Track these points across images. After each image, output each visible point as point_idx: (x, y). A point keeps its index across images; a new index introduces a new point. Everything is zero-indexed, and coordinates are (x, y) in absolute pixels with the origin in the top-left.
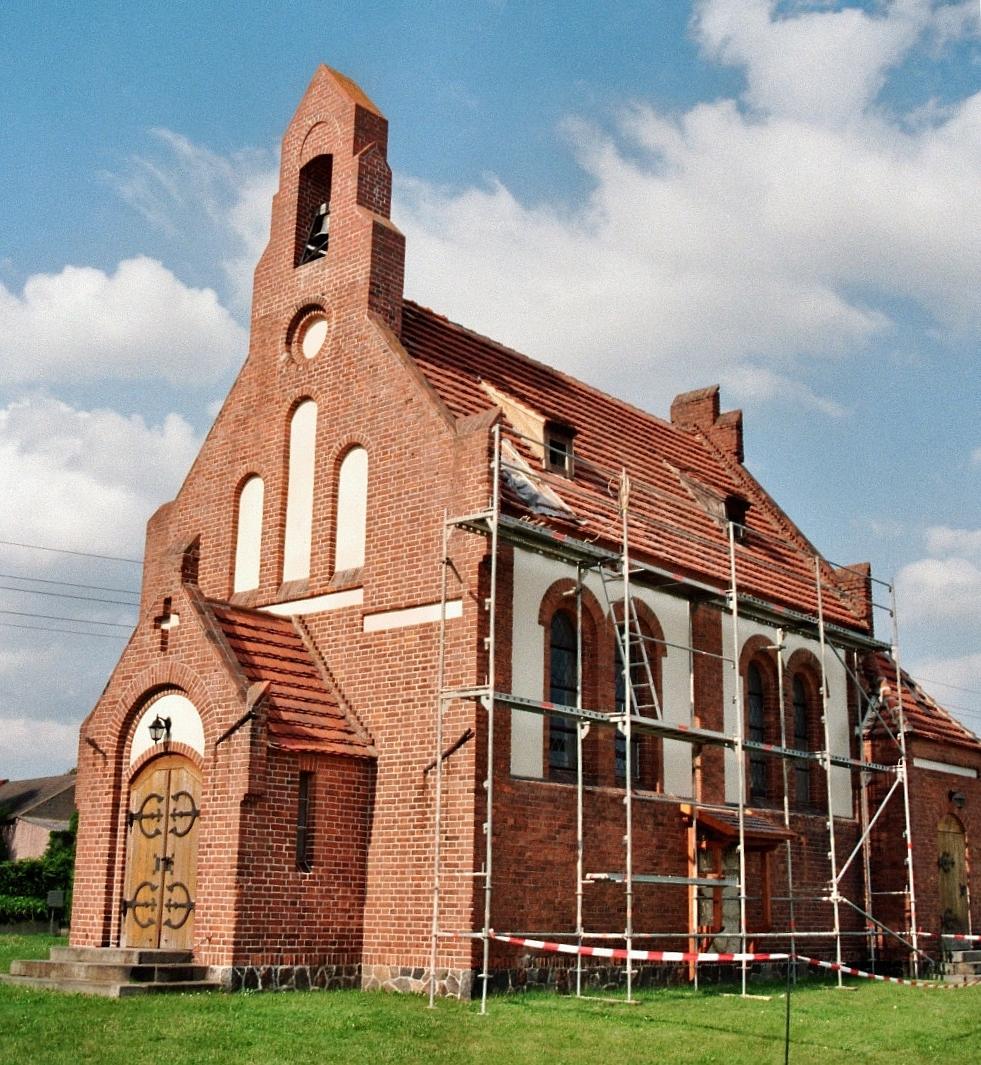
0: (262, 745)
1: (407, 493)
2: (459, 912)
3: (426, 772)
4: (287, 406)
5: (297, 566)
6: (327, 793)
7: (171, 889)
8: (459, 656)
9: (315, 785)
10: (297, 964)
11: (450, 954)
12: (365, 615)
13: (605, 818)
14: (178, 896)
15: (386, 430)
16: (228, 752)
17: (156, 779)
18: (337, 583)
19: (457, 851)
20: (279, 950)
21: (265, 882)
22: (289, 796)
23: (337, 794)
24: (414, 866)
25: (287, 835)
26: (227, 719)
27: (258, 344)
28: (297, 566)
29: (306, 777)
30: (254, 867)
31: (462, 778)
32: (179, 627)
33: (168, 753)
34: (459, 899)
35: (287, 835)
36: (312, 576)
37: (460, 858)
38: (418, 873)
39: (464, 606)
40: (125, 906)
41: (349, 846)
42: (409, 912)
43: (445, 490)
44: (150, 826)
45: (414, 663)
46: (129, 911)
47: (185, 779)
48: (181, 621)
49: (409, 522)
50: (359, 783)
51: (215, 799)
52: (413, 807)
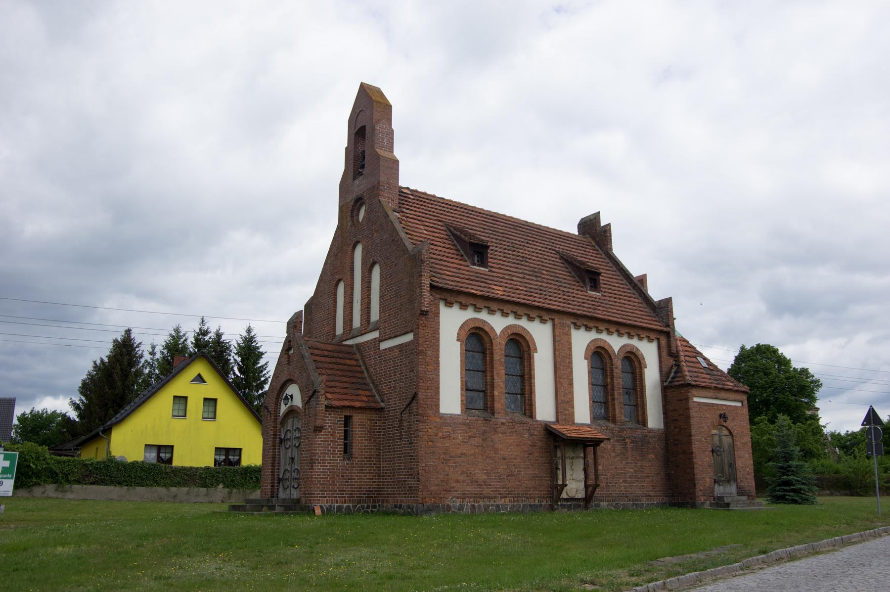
5: (357, 323)
12: (381, 341)
14: (295, 475)
18: (371, 327)
28: (357, 323)
29: (347, 420)
40: (280, 480)
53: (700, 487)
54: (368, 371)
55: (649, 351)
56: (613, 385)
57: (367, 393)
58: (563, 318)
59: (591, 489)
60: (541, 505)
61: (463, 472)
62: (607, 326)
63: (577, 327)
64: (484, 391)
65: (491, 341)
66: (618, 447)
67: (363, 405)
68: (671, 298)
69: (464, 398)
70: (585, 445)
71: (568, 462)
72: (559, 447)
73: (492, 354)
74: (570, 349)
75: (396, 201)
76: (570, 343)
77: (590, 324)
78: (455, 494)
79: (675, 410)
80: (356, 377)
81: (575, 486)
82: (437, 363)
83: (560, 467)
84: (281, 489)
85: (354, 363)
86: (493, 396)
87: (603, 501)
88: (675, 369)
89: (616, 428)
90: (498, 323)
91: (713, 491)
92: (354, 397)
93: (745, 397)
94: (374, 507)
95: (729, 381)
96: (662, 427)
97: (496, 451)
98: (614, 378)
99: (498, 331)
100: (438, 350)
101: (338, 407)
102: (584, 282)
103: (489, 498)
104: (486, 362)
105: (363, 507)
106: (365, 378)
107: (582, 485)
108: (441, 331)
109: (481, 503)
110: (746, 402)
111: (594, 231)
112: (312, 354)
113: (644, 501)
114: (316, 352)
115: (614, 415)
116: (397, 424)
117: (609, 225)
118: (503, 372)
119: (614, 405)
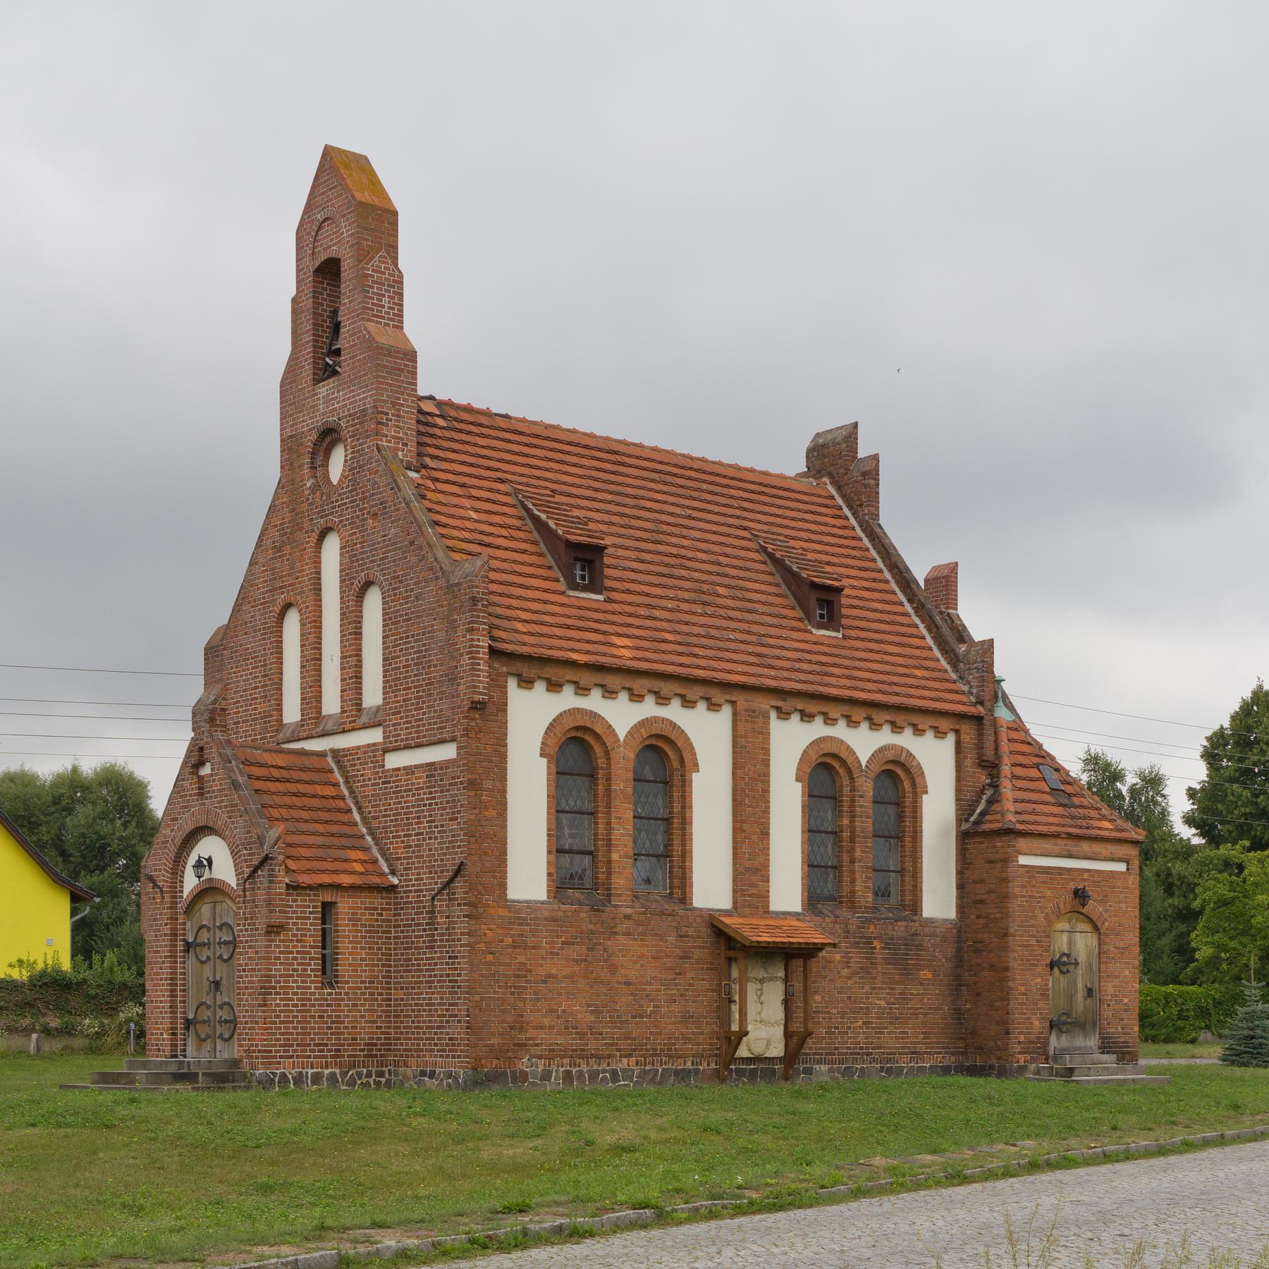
0: (280, 882)
1: (413, 636)
2: (459, 1022)
3: (433, 899)
4: (315, 536)
5: (331, 703)
6: (349, 920)
7: (221, 1007)
8: (456, 795)
9: (337, 913)
10: (327, 1067)
11: (453, 1057)
12: (386, 751)
13: (616, 933)
14: (223, 1014)
15: (395, 572)
16: (253, 889)
17: (205, 910)
19: (456, 969)
20: (309, 1057)
21: (292, 999)
22: (311, 924)
23: (360, 920)
24: (427, 982)
25: (311, 959)
26: (251, 860)
27: (288, 464)
28: (331, 703)
29: (327, 909)
30: (281, 988)
31: (459, 905)
32: (211, 775)
33: (210, 890)
34: (459, 1010)
35: (311, 959)
36: (343, 712)
37: (459, 975)
38: (430, 988)
39: (458, 748)
40: (188, 1023)
41: (374, 965)
42: (424, 1022)
43: (441, 635)
44: (205, 953)
45: (423, 799)
46: (191, 1027)
47: (227, 910)
48: (212, 770)
49: (416, 664)
50: (382, 909)
51: (246, 930)
52: (425, 930)
53: (1019, 1035)
54: (359, 809)
55: (935, 758)
56: (853, 832)
57: (360, 855)
58: (754, 698)
59: (796, 1040)
60: (697, 1071)
61: (551, 1011)
62: (846, 709)
63: (784, 715)
64: (590, 853)
65: (607, 753)
66: (857, 959)
67: (357, 880)
68: (991, 641)
69: (553, 871)
70: (793, 956)
71: (751, 988)
72: (736, 959)
73: (609, 779)
74: (766, 763)
75: (412, 447)
76: (766, 751)
77: (811, 708)
78: (534, 1050)
79: (982, 881)
80: (337, 823)
81: (764, 1031)
82: (502, 805)
83: (737, 998)
84: (191, 1042)
85: (329, 791)
86: (609, 862)
87: (819, 1062)
88: (989, 792)
89: (854, 919)
90: (622, 715)
91: (1046, 1044)
92: (337, 866)
93: (1133, 852)
94: (381, 1074)
95: (1104, 818)
96: (952, 914)
97: (613, 968)
98: (858, 816)
99: (622, 735)
100: (504, 779)
101: (310, 887)
102: (808, 615)
103: (597, 1057)
104: (596, 796)
105: (360, 1075)
106: (362, 837)
107: (780, 1031)
108: (510, 740)
109: (585, 1068)
110: (1136, 863)
111: (840, 465)
112: (250, 777)
113: (904, 1062)
114: (257, 771)
115: (853, 893)
116: (424, 919)
117: (875, 458)
118: (629, 814)
119: (853, 872)
